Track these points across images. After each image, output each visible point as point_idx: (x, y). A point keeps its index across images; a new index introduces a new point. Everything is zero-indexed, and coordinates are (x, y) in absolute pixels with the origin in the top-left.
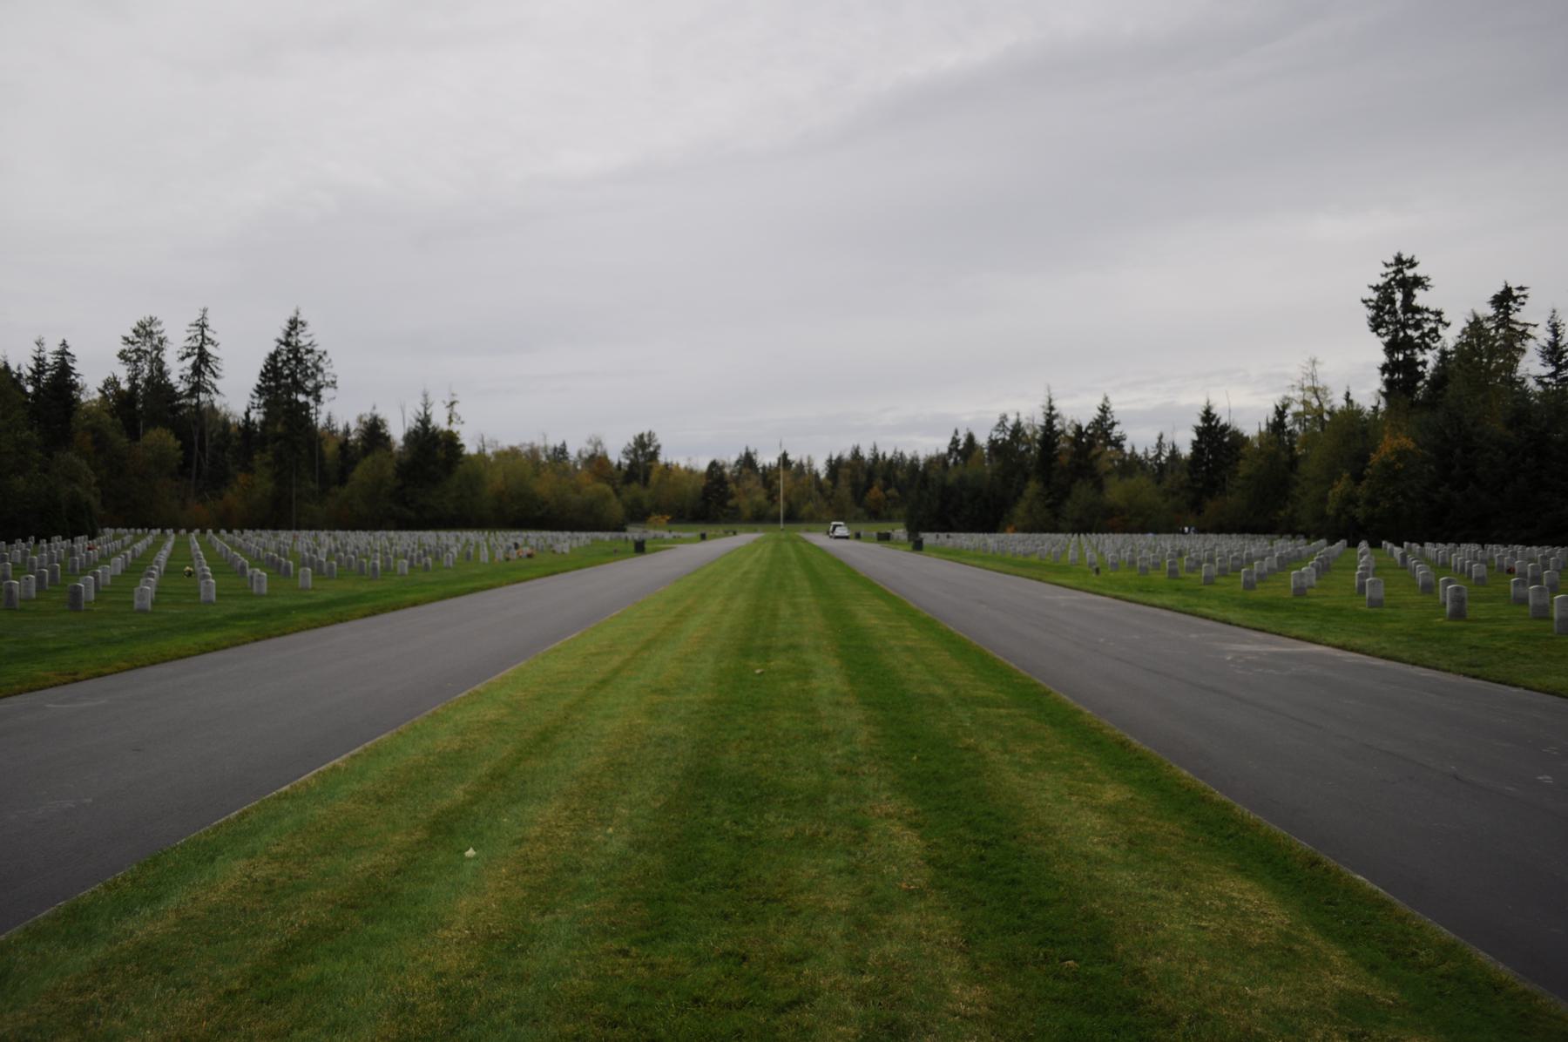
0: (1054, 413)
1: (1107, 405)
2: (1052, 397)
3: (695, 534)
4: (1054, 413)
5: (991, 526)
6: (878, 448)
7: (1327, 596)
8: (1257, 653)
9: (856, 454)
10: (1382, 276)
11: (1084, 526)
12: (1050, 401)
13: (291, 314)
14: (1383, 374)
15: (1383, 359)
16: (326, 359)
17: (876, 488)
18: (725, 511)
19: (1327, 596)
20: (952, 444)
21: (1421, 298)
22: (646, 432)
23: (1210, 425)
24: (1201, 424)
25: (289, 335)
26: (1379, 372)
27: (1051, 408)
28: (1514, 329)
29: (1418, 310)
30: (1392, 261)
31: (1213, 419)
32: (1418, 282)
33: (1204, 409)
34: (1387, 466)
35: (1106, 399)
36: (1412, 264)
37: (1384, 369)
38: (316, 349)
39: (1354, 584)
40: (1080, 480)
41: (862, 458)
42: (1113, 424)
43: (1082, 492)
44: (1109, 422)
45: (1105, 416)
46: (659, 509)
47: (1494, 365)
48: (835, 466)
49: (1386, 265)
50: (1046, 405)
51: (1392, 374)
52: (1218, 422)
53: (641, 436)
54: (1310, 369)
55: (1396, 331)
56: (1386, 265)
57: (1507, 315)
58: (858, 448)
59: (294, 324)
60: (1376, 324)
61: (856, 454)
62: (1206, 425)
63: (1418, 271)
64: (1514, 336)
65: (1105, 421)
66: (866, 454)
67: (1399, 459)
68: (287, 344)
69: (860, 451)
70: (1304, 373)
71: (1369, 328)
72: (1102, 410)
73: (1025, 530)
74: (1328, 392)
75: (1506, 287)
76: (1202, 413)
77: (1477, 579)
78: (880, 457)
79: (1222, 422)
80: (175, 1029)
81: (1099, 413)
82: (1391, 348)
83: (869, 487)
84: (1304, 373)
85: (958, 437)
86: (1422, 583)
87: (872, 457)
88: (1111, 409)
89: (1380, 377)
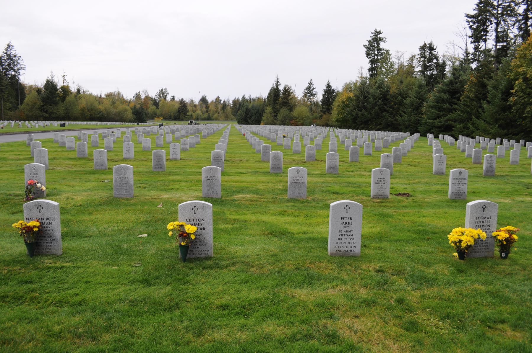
3: (173, 123)
5: (258, 122)
8: (123, 164)
10: (371, 37)
11: (283, 123)
13: (8, 43)
14: (369, 72)
15: (369, 66)
16: (21, 59)
18: (186, 116)
21: (382, 45)
22: (164, 89)
25: (7, 50)
26: (368, 71)
27: (278, 82)
29: (381, 50)
30: (374, 32)
32: (381, 39)
36: (380, 33)
37: (369, 70)
38: (17, 55)
39: (527, 154)
42: (313, 89)
43: (284, 111)
46: (161, 115)
48: (235, 102)
49: (372, 33)
51: (372, 72)
53: (162, 90)
55: (374, 56)
56: (372, 33)
59: (9, 46)
60: (368, 55)
63: (381, 36)
66: (247, 97)
68: (6, 53)
72: (309, 84)
75: (368, 41)
77: (377, 148)
79: (333, 88)
82: (372, 62)
89: (368, 73)
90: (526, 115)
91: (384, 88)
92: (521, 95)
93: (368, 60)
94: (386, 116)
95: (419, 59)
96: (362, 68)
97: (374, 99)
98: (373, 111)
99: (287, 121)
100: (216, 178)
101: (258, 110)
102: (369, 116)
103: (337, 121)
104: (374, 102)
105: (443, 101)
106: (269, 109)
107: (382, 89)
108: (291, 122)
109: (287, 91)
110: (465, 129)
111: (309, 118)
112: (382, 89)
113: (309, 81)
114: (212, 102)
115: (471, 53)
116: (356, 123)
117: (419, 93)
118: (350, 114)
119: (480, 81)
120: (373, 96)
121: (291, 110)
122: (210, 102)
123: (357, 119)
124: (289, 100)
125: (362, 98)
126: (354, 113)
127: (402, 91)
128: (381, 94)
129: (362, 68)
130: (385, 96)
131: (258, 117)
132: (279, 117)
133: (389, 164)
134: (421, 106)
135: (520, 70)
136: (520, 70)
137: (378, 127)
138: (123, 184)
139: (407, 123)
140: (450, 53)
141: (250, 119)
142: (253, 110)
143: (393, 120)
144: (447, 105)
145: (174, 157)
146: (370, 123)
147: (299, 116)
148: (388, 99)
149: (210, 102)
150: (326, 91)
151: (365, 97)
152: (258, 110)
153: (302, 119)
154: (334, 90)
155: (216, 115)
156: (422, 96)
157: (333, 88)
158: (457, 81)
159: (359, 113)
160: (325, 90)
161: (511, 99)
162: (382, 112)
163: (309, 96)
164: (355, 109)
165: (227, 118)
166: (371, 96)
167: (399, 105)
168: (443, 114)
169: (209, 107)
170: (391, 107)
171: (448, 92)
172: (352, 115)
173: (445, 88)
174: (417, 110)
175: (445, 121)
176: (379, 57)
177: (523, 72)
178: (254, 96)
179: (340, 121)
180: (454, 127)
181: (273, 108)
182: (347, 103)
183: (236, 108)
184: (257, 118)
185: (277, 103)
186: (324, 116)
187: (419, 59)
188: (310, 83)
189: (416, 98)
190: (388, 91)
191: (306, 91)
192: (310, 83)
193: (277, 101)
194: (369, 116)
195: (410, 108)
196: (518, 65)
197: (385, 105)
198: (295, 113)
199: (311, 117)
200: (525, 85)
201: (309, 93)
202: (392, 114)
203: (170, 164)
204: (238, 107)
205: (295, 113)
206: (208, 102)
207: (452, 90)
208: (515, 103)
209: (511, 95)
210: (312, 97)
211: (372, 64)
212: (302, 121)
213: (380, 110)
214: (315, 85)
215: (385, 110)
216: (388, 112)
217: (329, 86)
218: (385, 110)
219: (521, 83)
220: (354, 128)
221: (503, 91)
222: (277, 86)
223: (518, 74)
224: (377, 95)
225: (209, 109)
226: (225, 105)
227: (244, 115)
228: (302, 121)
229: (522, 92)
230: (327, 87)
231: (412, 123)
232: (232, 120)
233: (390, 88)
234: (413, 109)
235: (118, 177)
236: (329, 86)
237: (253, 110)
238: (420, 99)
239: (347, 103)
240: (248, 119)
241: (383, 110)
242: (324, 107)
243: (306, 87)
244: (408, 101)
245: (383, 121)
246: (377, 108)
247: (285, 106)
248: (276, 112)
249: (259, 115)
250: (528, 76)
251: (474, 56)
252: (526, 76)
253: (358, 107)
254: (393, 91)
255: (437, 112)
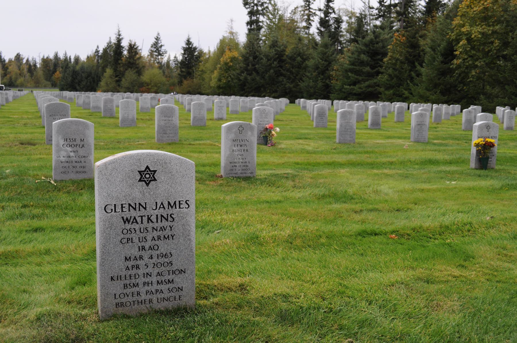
0: (121, 37)
1: (159, 37)
2: (120, 30)
4: (121, 37)
6: (67, 53)
7: (447, 128)
9: (56, 56)
12: (119, 31)
14: (247, 26)
15: (247, 19)
17: (58, 72)
19: (447, 128)
20: (96, 52)
23: (189, 46)
24: (185, 46)
26: (245, 25)
27: (119, 35)
28: (311, 12)
31: (190, 44)
33: (187, 39)
34: (226, 64)
35: (158, 34)
37: (248, 23)
40: (129, 69)
41: (60, 58)
42: (161, 46)
43: (130, 75)
44: (160, 45)
45: (158, 42)
47: (255, 18)
50: (117, 34)
51: (251, 26)
52: (192, 45)
54: (231, 23)
55: (253, 6)
57: (309, 5)
58: (57, 53)
61: (56, 56)
62: (187, 46)
64: (311, 14)
65: (158, 44)
66: (61, 56)
67: (231, 61)
69: (58, 55)
70: (228, 25)
71: (243, 5)
72: (156, 39)
73: (105, 91)
74: (238, 34)
76: (186, 41)
78: (68, 58)
79: (194, 46)
80: (258, 268)
81: (155, 40)
82: (251, 13)
83: (55, 71)
84: (228, 25)
85: (99, 50)
86: (194, 118)
87: (64, 58)
88: (161, 39)
90: (472, 79)
91: (280, 47)
92: (466, 57)
93: (246, 11)
94: (283, 81)
95: (302, 12)
96: (232, 21)
97: (268, 60)
98: (267, 75)
99: (136, 88)
100: (425, 123)
101: (91, 73)
102: (262, 81)
103: (219, 87)
104: (268, 63)
105: (362, 63)
106: (109, 71)
107: (277, 48)
108: (141, 89)
109: (133, 48)
110: (395, 96)
111: (164, 85)
112: (277, 48)
113: (155, 35)
114: (10, 61)
115: (375, 7)
116: (244, 90)
117: (325, 53)
118: (237, 79)
119: (410, 41)
120: (267, 56)
121: (139, 73)
122: (7, 61)
123: (245, 85)
124: (136, 60)
125: (251, 58)
126: (242, 78)
127: (301, 50)
128: (276, 54)
129: (232, 21)
130: (280, 56)
131: (91, 83)
132: (124, 82)
133: (470, 119)
134: (327, 70)
135: (463, 30)
136: (463, 30)
137: (273, 95)
138: (347, 129)
139: (312, 90)
140: (343, 7)
141: (79, 85)
142: (83, 72)
143: (292, 86)
144: (367, 69)
145: (220, 117)
146: (262, 89)
147: (151, 81)
148: (285, 60)
149: (7, 61)
150: (185, 50)
151: (255, 57)
152: (91, 73)
153: (156, 86)
154: (195, 49)
155: (21, 80)
156: (328, 57)
157: (194, 46)
158: (378, 40)
159: (249, 78)
160: (184, 48)
161: (455, 61)
162: (278, 76)
163: (156, 55)
164: (243, 72)
165: (37, 85)
166: (264, 56)
167: (298, 68)
168: (363, 79)
169: (7, 68)
170: (288, 70)
171: (368, 53)
172: (240, 80)
173: (363, 48)
174: (323, 74)
175: (366, 87)
176: (260, 8)
177: (467, 32)
178: (72, 55)
179: (222, 88)
180: (381, 94)
181: (115, 70)
182: (231, 64)
183: (49, 70)
184: (89, 83)
185: (120, 64)
186: (185, 82)
187: (302, 12)
188: (157, 39)
189: (321, 59)
190: (284, 51)
191: (153, 49)
192: (157, 39)
193: (120, 62)
194: (262, 81)
195: (314, 72)
196: (461, 24)
197: (281, 67)
198: (146, 77)
199: (167, 83)
200: (469, 46)
201: (156, 52)
202: (289, 78)
203: (102, 135)
204: (51, 69)
205: (146, 77)
206: (4, 61)
207: (373, 50)
208: (459, 67)
209: (454, 57)
210: (159, 57)
211: (251, 17)
212: (155, 88)
213: (275, 74)
214: (163, 41)
215: (282, 75)
216: (285, 77)
217: (189, 42)
218: (282, 75)
219: (465, 45)
220: (242, 95)
221: (443, 52)
222: (119, 41)
223: (460, 35)
224: (272, 55)
225: (8, 70)
226: (31, 68)
227: (70, 79)
228: (155, 88)
229: (466, 54)
230: (187, 44)
231: (317, 90)
232: (45, 87)
233: (286, 47)
234: (318, 72)
235: (344, 121)
236: (189, 42)
237: (83, 72)
238: (326, 61)
239: (231, 64)
240: (77, 85)
241: (279, 74)
242: (183, 70)
243: (152, 43)
244: (310, 63)
245: (280, 88)
246: (272, 71)
247: (131, 68)
248: (118, 76)
249: (91, 80)
250: (473, 36)
251: (379, 12)
252: (470, 37)
253: (247, 70)
254: (289, 51)
255: (356, 77)
